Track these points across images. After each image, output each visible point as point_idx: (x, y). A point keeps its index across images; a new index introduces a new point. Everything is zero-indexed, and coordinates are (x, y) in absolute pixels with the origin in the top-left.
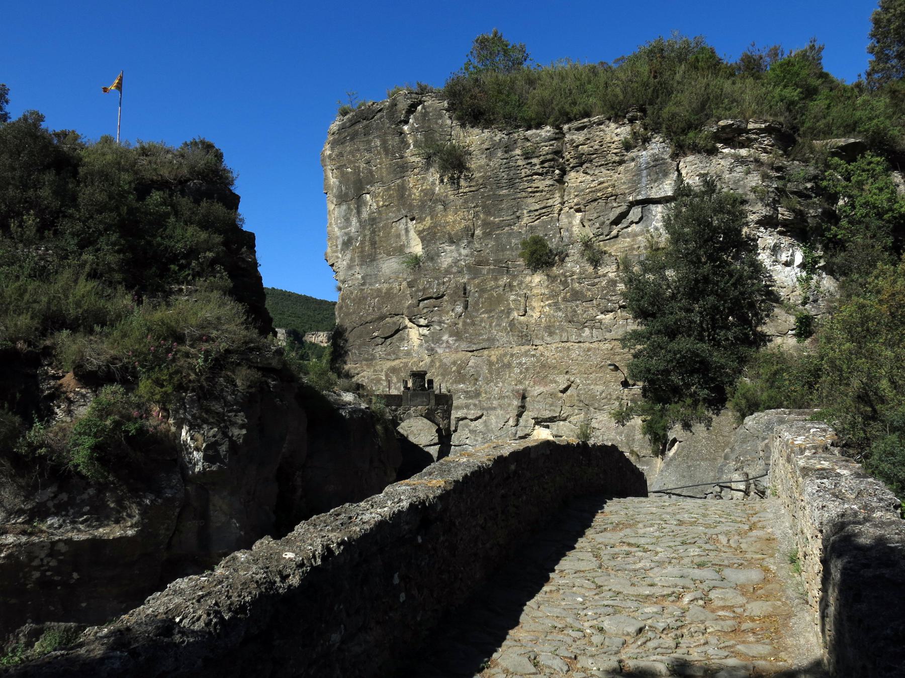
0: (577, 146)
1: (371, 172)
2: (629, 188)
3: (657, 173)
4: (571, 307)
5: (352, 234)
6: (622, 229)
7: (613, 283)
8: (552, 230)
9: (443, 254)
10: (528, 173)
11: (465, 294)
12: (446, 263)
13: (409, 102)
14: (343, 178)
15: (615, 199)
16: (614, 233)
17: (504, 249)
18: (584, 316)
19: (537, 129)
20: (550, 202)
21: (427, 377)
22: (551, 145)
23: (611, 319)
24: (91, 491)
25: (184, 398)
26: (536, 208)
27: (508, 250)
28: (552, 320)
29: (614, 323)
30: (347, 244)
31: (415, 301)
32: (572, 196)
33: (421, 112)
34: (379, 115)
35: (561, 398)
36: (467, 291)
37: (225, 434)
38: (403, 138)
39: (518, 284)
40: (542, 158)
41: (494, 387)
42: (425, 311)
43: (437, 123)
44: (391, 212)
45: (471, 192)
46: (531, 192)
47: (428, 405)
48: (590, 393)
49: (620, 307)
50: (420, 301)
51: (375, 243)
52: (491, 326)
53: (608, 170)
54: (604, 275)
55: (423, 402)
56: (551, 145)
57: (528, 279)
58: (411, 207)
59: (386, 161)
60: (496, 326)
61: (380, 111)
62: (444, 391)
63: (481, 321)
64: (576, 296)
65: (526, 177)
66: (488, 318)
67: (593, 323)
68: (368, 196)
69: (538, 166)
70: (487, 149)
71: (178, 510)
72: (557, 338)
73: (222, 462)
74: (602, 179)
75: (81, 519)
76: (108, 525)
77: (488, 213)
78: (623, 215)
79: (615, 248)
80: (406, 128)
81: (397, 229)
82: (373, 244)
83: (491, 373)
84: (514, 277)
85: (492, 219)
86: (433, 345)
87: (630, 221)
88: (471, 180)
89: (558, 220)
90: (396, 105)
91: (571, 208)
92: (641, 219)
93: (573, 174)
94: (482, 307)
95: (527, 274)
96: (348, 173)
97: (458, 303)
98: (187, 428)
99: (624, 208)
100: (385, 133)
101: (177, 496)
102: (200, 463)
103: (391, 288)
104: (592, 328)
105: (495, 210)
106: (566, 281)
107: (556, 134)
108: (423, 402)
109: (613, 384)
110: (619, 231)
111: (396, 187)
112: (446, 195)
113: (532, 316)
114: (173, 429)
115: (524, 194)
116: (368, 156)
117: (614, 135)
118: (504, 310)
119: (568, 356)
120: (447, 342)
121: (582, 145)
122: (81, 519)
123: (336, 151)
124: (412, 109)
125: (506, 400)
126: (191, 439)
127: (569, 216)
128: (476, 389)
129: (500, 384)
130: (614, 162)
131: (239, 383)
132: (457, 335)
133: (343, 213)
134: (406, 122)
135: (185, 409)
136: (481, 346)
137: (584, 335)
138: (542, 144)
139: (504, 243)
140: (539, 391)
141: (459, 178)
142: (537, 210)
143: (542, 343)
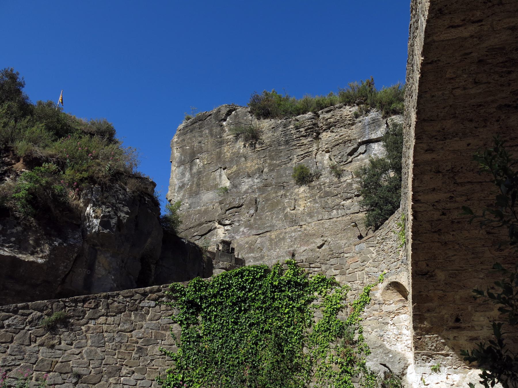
0: (327, 120)
1: (201, 147)
2: (358, 136)
3: (375, 126)
4: (324, 201)
5: (185, 182)
6: (354, 158)
7: (351, 184)
8: (311, 163)
9: (243, 184)
10: (297, 136)
11: (256, 203)
12: (245, 188)
13: (228, 109)
14: (183, 152)
15: (350, 143)
16: (350, 160)
17: (281, 176)
18: (333, 204)
19: (303, 114)
20: (311, 149)
21: (231, 246)
22: (312, 121)
23: (350, 202)
24: (19, 229)
25: (92, 188)
26: (302, 153)
27: (284, 177)
28: (312, 209)
29: (352, 204)
30: (181, 188)
31: (223, 211)
32: (324, 144)
33: (234, 115)
34: (209, 117)
35: (318, 251)
36: (257, 202)
37: (116, 214)
38: (223, 128)
39: (290, 194)
40: (306, 128)
41: (274, 252)
42: (230, 215)
43: (243, 119)
44: (211, 167)
45: (262, 150)
46: (299, 146)
47: (231, 263)
48: (337, 245)
49: (355, 196)
50: (227, 210)
51: (200, 185)
52: (272, 218)
53: (346, 128)
54: (345, 181)
55: (228, 260)
56: (312, 121)
57: (297, 190)
58: (225, 162)
59: (211, 140)
60: (275, 218)
61: (210, 115)
62: (240, 257)
63: (266, 217)
64: (327, 194)
65: (296, 138)
66: (270, 214)
67: (338, 206)
68: (198, 160)
69: (304, 132)
70: (273, 128)
71: (76, 255)
72: (316, 219)
73: (111, 229)
74: (342, 134)
75: (7, 245)
76: (26, 254)
77: (272, 159)
78: (355, 150)
79: (350, 168)
80: (224, 123)
81: (214, 175)
82: (198, 185)
83: (271, 245)
84: (288, 191)
85: (275, 162)
86: (233, 235)
87: (359, 153)
88: (262, 144)
89: (315, 158)
90: (220, 112)
91: (323, 151)
92: (365, 151)
93: (324, 134)
94: (267, 209)
95: (296, 188)
96: (186, 149)
97: (252, 208)
98: (92, 205)
99: (355, 146)
100: (212, 126)
101: (77, 244)
102: (97, 227)
103: (208, 208)
104: (338, 210)
105: (277, 157)
106: (321, 188)
107: (314, 116)
108: (228, 260)
109: (352, 238)
110: (352, 159)
111: (216, 153)
112: (247, 153)
113: (299, 210)
114: (82, 205)
115: (294, 147)
116: (200, 139)
117: (348, 112)
118: (281, 208)
119: (323, 227)
120: (243, 231)
121: (330, 118)
122: (7, 245)
123: (181, 139)
124: (229, 113)
125: (281, 258)
126: (93, 211)
127: (322, 155)
128: (261, 255)
129: (278, 250)
130: (349, 124)
131: (128, 190)
132: (250, 227)
133: (181, 171)
134: (225, 120)
135: (92, 194)
136: (266, 230)
137: (333, 214)
138: (306, 121)
139: (281, 173)
140: (304, 249)
141: (255, 143)
142: (302, 155)
143: (305, 223)
